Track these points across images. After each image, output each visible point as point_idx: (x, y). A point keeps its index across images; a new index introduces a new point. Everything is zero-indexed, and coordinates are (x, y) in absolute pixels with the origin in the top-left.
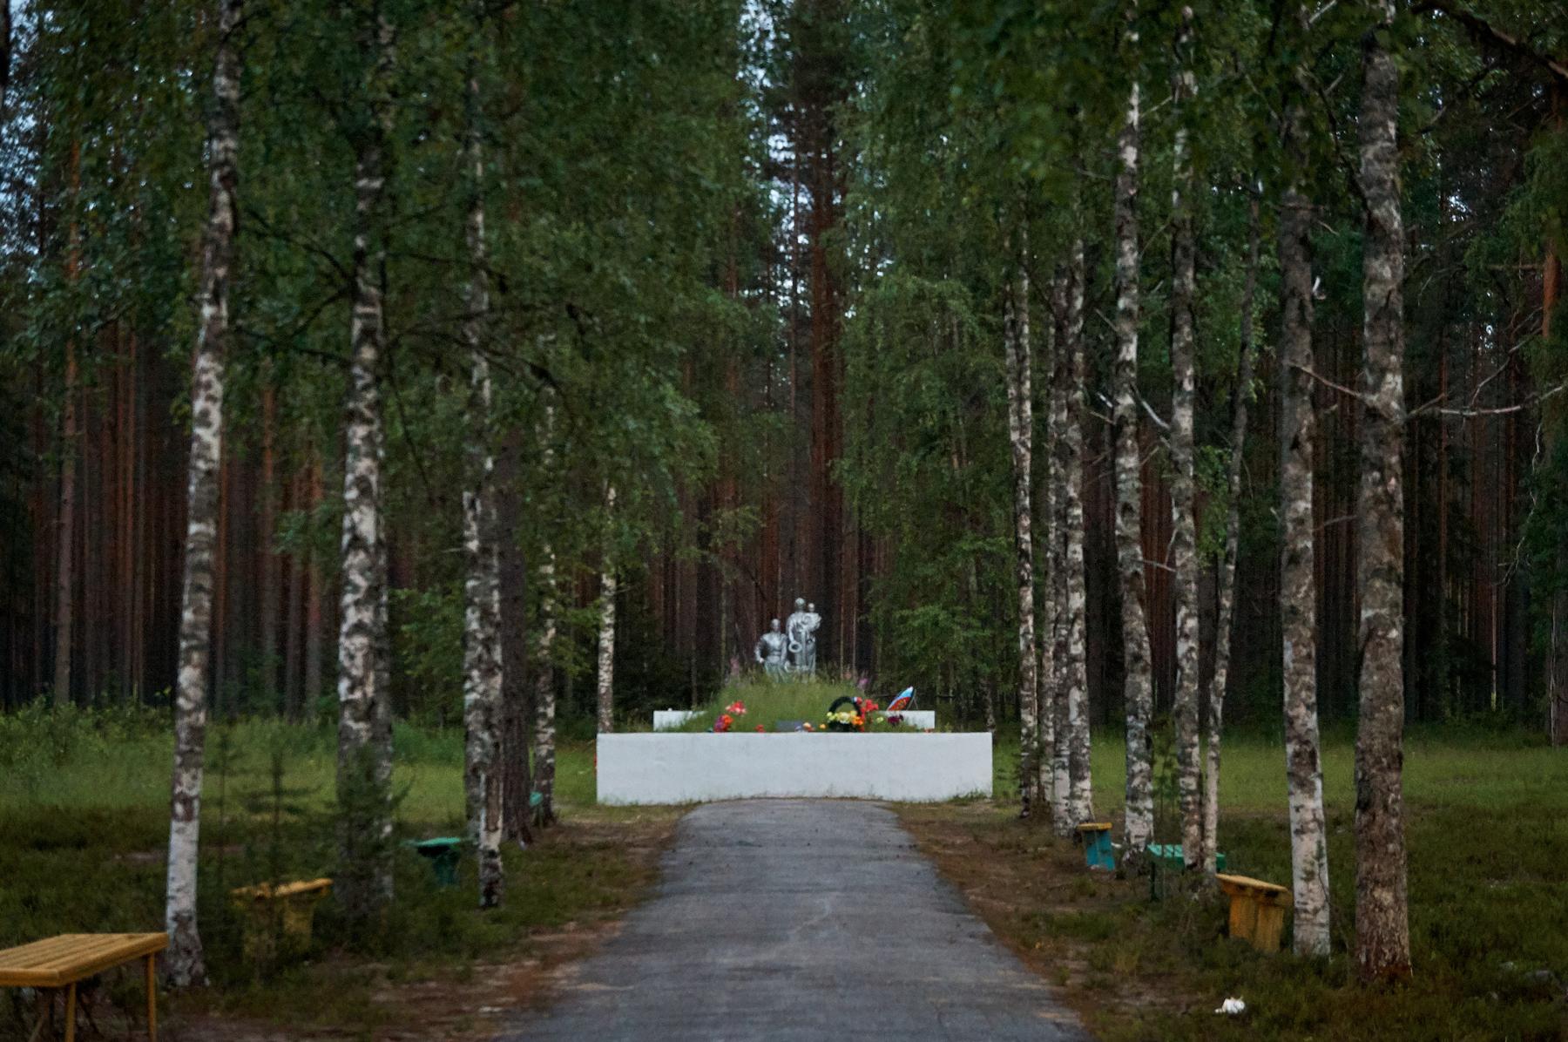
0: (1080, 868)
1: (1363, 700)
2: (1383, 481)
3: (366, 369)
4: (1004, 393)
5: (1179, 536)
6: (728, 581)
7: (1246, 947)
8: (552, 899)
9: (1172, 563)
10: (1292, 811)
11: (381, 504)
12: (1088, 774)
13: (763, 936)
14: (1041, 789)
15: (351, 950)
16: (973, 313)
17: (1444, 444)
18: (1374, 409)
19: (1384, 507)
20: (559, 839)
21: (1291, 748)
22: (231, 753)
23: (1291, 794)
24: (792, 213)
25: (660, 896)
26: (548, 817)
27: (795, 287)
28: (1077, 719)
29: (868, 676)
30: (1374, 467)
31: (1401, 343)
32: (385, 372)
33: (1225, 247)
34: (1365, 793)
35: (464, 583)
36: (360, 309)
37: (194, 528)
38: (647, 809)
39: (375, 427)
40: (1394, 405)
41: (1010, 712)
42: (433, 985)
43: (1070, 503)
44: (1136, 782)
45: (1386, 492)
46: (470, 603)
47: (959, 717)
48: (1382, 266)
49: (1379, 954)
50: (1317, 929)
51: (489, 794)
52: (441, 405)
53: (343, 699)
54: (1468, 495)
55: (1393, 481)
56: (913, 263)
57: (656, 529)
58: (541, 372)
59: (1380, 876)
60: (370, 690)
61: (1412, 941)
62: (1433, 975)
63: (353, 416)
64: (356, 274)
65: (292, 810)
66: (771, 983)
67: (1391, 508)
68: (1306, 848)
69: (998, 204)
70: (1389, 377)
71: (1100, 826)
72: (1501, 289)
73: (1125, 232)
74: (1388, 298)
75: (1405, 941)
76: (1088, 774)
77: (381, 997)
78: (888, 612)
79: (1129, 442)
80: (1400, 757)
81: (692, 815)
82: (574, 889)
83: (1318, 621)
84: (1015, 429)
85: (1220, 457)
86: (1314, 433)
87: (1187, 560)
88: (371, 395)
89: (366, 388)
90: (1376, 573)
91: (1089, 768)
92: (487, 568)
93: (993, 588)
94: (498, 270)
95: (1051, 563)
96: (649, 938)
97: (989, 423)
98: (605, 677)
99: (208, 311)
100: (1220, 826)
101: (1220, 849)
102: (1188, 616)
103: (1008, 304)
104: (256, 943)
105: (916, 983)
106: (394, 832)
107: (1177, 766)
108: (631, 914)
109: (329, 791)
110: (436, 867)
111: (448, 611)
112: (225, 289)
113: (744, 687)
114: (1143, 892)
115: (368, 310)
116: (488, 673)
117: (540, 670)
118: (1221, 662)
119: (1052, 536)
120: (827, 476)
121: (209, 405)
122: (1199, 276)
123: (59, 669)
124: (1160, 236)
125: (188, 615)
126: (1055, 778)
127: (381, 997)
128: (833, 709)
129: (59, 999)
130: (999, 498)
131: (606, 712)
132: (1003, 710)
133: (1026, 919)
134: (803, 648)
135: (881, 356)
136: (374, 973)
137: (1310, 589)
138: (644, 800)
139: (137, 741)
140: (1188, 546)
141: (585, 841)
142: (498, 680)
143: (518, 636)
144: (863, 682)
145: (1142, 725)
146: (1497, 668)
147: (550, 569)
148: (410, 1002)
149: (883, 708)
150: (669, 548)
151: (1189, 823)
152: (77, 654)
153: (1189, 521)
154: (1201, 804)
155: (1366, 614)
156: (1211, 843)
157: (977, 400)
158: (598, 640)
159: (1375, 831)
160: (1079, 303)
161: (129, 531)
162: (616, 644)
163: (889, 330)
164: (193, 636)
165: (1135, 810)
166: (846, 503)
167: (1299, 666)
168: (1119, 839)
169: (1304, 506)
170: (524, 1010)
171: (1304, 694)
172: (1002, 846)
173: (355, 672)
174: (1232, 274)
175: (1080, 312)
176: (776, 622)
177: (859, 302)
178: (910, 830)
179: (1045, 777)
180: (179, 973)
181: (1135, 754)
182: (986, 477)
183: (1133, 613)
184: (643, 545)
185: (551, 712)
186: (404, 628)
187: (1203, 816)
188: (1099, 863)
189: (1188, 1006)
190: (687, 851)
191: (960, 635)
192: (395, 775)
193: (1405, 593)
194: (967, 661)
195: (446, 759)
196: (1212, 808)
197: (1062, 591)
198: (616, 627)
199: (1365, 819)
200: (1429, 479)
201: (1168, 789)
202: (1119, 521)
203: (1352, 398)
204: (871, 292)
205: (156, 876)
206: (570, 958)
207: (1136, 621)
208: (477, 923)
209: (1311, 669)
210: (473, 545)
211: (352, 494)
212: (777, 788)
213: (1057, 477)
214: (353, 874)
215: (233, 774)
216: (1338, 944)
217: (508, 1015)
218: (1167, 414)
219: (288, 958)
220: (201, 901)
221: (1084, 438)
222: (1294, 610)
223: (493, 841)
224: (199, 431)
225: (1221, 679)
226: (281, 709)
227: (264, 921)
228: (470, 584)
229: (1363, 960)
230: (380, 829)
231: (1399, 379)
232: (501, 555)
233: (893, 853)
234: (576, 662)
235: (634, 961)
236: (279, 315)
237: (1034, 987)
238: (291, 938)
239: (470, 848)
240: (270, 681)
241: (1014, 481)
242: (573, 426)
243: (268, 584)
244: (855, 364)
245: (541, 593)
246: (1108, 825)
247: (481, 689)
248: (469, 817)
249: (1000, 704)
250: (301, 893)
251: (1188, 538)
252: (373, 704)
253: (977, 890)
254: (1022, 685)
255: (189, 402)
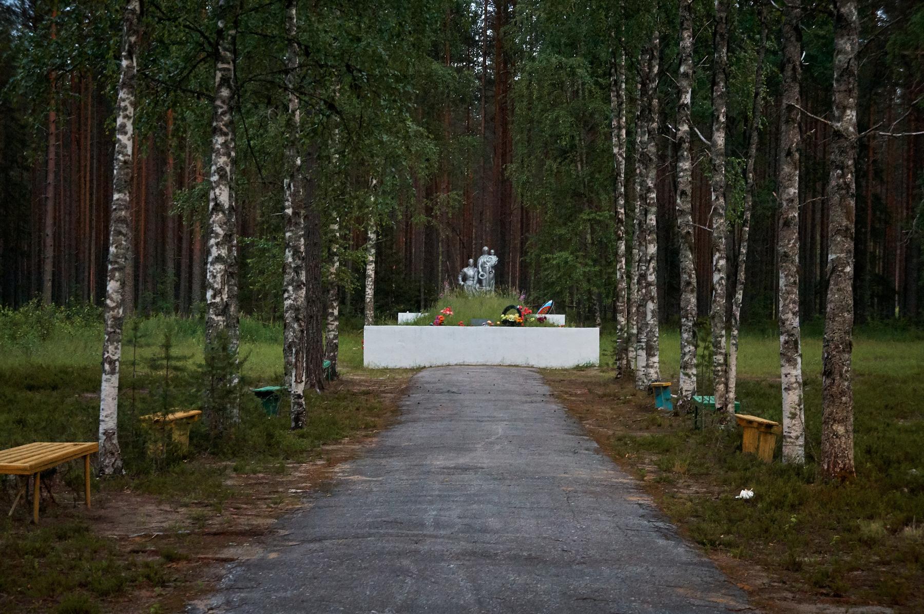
0: (651, 409)
1: (828, 310)
2: (843, 176)
3: (223, 102)
4: (610, 125)
5: (715, 209)
6: (443, 236)
7: (753, 458)
8: (335, 423)
9: (711, 226)
10: (783, 377)
11: (233, 184)
12: (657, 353)
13: (461, 448)
14: (628, 362)
15: (213, 453)
16: (591, 77)
17: (872, 159)
18: (839, 131)
19: (844, 192)
20: (341, 388)
21: (783, 338)
22: (139, 334)
23: (782, 366)
24: (483, 17)
25: (400, 423)
26: (333, 374)
27: (484, 61)
28: (651, 320)
29: (525, 294)
30: (837, 167)
31: (856, 91)
32: (234, 107)
33: (745, 37)
34: (829, 366)
35: (284, 234)
36: (220, 66)
37: (116, 196)
38: (393, 370)
39: (229, 137)
40: (851, 129)
41: (609, 315)
42: (261, 475)
43: (649, 190)
44: (686, 358)
45: (845, 183)
46: (288, 246)
47: (579, 318)
48: (846, 43)
49: (836, 464)
50: (797, 448)
51: (297, 360)
52: (272, 129)
53: (209, 302)
54: (884, 191)
55: (849, 176)
56: (556, 47)
57: (400, 204)
58: (331, 106)
59: (837, 417)
60: (225, 297)
61: (855, 457)
62: (868, 477)
63: (216, 131)
64: (218, 44)
65: (176, 368)
66: (466, 477)
67: (848, 193)
68: (791, 399)
69: (608, 10)
70: (848, 112)
71: (664, 384)
72: (907, 65)
73: (685, 26)
74: (849, 63)
75: (851, 456)
76: (657, 353)
77: (229, 482)
78: (538, 256)
79: (686, 153)
80: (850, 344)
81: (420, 374)
82: (348, 418)
83: (800, 262)
84: (616, 146)
85: (739, 163)
86: (800, 147)
87: (719, 224)
88: (226, 118)
89: (223, 113)
90: (838, 232)
91: (658, 350)
92: (297, 224)
93: (601, 242)
94: (306, 43)
95: (636, 226)
96: (393, 447)
97: (600, 143)
98: (370, 292)
99: (125, 63)
100: (737, 386)
101: (736, 399)
102: (720, 258)
103: (613, 70)
104: (155, 448)
105: (554, 478)
106: (239, 382)
107: (712, 348)
108: (383, 433)
109: (200, 358)
110: (265, 405)
111: (275, 251)
112: (137, 50)
113: (452, 299)
114: (690, 424)
115: (225, 66)
116: (298, 287)
117: (330, 287)
118: (740, 286)
119: (637, 210)
120: (503, 175)
121: (126, 120)
122: (729, 54)
123: (45, 283)
124: (705, 29)
125: (112, 249)
126: (637, 355)
127: (229, 482)
128: (505, 313)
129: (31, 481)
130: (605, 190)
131: (370, 313)
132: (605, 315)
133: (620, 439)
134: (487, 276)
135: (536, 103)
136: (226, 467)
137: (796, 242)
138: (391, 366)
139: (91, 326)
140: (720, 215)
141: (356, 389)
142: (303, 292)
143: (316, 266)
144: (522, 297)
145: (691, 324)
146: (899, 293)
147: (336, 227)
148: (246, 485)
149: (533, 313)
150: (408, 216)
151: (718, 383)
152: (56, 276)
153: (722, 200)
154: (726, 372)
155: (831, 257)
156: (732, 395)
157: (592, 130)
158: (365, 270)
159: (835, 389)
160: (656, 70)
161: (88, 202)
162: (376, 273)
163: (541, 87)
164: (116, 262)
165: (686, 374)
166: (514, 191)
167: (789, 288)
168: (676, 392)
169: (793, 191)
170: (316, 492)
171: (791, 306)
172: (605, 395)
173: (216, 286)
174: (748, 54)
175: (656, 75)
176: (471, 261)
177: (522, 70)
178: (550, 385)
179: (631, 355)
180: (107, 467)
181: (687, 341)
182: (597, 176)
183: (686, 257)
184: (392, 215)
185: (336, 312)
186: (249, 261)
187: (727, 379)
188: (663, 406)
189: (719, 494)
190: (416, 396)
191: (581, 270)
192: (241, 349)
193: (855, 244)
194: (585, 285)
195: (274, 340)
196: (733, 374)
197: (643, 243)
198: (376, 263)
199: (828, 382)
200: (861, 180)
201: (707, 361)
202: (678, 201)
203: (826, 124)
204: (530, 63)
205: (93, 408)
206: (345, 460)
207: (688, 261)
208: (290, 438)
209: (796, 290)
210: (289, 211)
211: (215, 178)
212: (471, 360)
213: (641, 175)
214: (214, 407)
215: (141, 347)
216: (809, 457)
217: (306, 495)
218: (709, 137)
219: (173, 457)
220: (120, 425)
221: (658, 151)
222: (786, 255)
223: (300, 389)
224: (120, 137)
225: (739, 296)
226: (177, 309)
227: (159, 436)
228: (288, 234)
229: (826, 467)
230: (230, 381)
231: (854, 113)
232: (306, 217)
233: (539, 399)
234: (352, 282)
235: (383, 462)
236: (171, 69)
237: (625, 481)
238: (176, 446)
239: (286, 393)
240: (170, 291)
241: (614, 179)
242: (350, 139)
243: (170, 234)
244: (520, 108)
245: (331, 241)
246: (669, 384)
247: (294, 298)
248: (286, 374)
249: (604, 310)
250: (182, 419)
251: (721, 211)
252: (227, 306)
253: (590, 421)
254: (618, 299)
255: (115, 121)
